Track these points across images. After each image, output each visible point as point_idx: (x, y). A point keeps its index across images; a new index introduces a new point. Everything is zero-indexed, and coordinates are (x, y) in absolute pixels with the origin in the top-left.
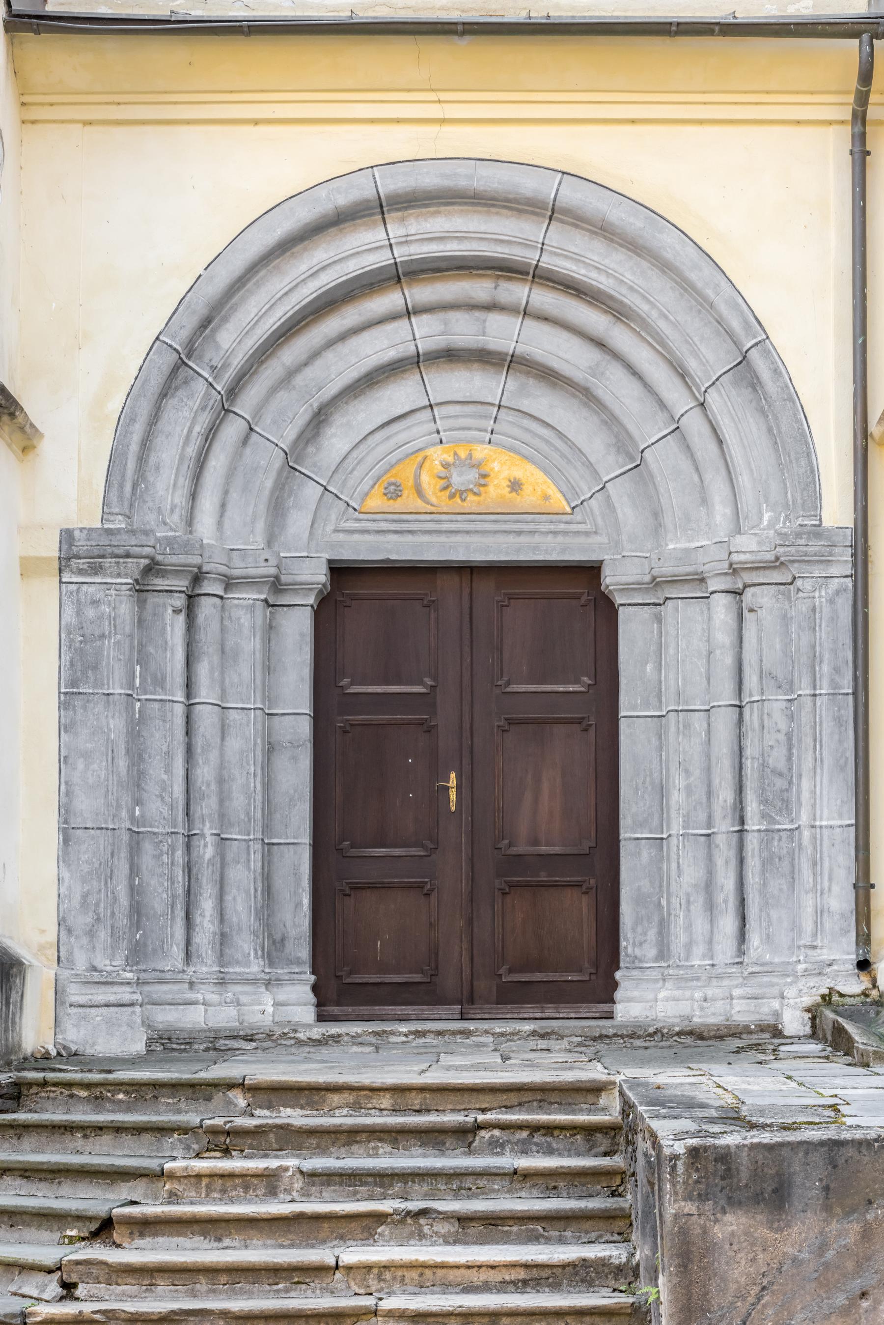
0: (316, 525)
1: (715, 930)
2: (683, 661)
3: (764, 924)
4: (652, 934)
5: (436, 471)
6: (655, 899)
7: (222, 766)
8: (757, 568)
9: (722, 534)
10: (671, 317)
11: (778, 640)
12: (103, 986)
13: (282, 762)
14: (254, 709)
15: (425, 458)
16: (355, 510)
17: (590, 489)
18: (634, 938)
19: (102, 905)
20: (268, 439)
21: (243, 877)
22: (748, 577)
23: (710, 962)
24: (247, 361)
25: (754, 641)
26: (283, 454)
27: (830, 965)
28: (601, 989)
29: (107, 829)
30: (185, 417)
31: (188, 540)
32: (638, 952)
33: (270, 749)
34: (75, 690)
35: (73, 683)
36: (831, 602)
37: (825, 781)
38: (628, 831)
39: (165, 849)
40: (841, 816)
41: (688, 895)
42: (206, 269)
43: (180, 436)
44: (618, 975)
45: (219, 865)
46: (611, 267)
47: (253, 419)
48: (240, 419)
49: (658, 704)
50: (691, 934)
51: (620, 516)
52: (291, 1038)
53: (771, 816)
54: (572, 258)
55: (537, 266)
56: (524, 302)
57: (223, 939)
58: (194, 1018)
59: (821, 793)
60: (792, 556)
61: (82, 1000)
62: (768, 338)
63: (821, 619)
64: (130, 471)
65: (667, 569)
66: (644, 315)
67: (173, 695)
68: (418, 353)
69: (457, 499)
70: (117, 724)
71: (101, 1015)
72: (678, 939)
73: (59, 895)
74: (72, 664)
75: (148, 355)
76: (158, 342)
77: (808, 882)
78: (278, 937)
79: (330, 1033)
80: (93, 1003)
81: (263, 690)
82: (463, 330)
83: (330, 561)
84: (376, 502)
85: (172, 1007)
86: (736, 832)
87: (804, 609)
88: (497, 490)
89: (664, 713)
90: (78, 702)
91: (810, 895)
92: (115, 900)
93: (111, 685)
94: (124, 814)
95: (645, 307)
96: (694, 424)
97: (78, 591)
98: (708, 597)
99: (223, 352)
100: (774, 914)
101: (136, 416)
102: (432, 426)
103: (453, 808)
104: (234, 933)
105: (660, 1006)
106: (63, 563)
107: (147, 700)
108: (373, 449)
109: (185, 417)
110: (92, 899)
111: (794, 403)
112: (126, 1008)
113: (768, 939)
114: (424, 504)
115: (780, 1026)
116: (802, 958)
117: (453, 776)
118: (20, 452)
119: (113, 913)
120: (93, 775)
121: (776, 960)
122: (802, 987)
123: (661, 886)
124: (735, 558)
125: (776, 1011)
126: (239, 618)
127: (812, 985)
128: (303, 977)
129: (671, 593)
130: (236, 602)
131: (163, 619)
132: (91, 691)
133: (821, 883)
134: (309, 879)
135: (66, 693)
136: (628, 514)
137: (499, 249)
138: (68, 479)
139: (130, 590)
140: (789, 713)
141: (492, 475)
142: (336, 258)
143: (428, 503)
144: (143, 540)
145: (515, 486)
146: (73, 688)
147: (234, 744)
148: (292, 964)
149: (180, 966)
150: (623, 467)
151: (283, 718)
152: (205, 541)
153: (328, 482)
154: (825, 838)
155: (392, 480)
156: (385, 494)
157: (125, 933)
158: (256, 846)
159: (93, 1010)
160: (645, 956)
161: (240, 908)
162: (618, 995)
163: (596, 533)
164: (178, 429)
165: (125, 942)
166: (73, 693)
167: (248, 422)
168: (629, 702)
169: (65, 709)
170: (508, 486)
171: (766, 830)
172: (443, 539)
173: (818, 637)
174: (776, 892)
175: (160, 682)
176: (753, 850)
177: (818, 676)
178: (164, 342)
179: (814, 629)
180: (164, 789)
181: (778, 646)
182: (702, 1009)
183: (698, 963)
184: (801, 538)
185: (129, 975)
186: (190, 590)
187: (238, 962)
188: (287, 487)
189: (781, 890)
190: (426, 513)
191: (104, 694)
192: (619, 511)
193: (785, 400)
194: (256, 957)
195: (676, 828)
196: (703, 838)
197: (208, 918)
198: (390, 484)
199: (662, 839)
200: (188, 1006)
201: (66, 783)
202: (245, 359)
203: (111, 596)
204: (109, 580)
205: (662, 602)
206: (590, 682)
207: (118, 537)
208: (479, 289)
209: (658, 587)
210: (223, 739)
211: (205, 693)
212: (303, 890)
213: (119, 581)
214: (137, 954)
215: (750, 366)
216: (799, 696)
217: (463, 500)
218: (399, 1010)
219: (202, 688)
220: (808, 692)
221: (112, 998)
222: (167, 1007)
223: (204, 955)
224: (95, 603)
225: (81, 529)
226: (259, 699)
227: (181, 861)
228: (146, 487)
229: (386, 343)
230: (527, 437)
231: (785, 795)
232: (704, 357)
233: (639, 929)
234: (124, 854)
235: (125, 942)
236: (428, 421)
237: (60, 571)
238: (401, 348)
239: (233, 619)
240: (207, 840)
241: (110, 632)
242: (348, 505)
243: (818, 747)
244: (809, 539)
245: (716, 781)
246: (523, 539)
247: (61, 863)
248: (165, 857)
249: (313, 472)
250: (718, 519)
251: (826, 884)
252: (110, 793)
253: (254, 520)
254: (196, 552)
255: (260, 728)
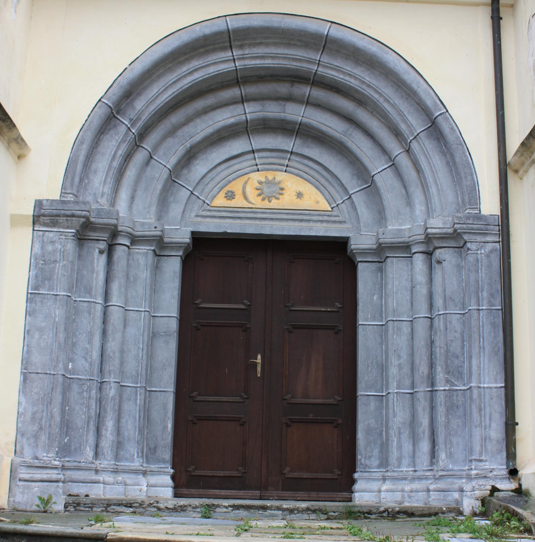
0: (185, 212)
1: (417, 449)
2: (396, 292)
3: (448, 446)
4: (376, 452)
5: (255, 186)
6: (378, 431)
7: (123, 343)
8: (442, 238)
9: (420, 220)
10: (391, 101)
11: (455, 279)
12: (40, 469)
13: (160, 343)
14: (144, 311)
15: (249, 178)
16: (208, 205)
17: (342, 198)
18: (366, 454)
19: (44, 420)
20: (160, 163)
21: (132, 409)
22: (437, 244)
23: (413, 469)
24: (150, 118)
25: (440, 279)
26: (168, 171)
27: (491, 472)
28: (347, 484)
29: (50, 374)
30: (113, 145)
31: (110, 210)
32: (367, 462)
33: (153, 336)
34: (36, 292)
35: (36, 288)
36: (488, 256)
37: (486, 361)
38: (364, 391)
39: (85, 388)
40: (496, 382)
41: (399, 429)
42: (130, 65)
43: (110, 155)
44: (356, 475)
45: (118, 401)
46: (357, 74)
47: (153, 151)
48: (145, 150)
49: (380, 318)
50: (401, 452)
51: (359, 212)
52: (155, 507)
53: (452, 382)
54: (335, 69)
55: (315, 73)
56: (307, 94)
57: (119, 445)
58: (97, 492)
59: (484, 367)
60: (464, 230)
61: (27, 476)
62: (447, 111)
63: (482, 265)
64: (79, 170)
65: (387, 239)
66: (376, 101)
67: (96, 299)
68: (247, 120)
69: (266, 201)
70: (59, 313)
71: (38, 487)
72: (394, 454)
73: (18, 413)
74: (36, 276)
75: (94, 108)
76: (100, 103)
77: (477, 420)
78: (152, 446)
79: (179, 504)
80: (34, 479)
81: (150, 303)
82: (273, 111)
83: (193, 233)
84: (220, 201)
85: (84, 484)
86: (429, 391)
87: (472, 260)
88: (287, 201)
89: (384, 323)
90: (38, 299)
91: (478, 429)
92: (52, 416)
93: (59, 290)
94: (61, 365)
95: (376, 96)
96: (404, 161)
97: (43, 235)
98: (411, 257)
99: (137, 111)
100: (454, 440)
101: (84, 140)
102: (253, 162)
103: (259, 375)
104: (126, 442)
105: (383, 495)
106: (35, 219)
107: (80, 301)
108: (220, 172)
109: (113, 145)
110: (38, 416)
111: (463, 146)
112: (53, 484)
113: (450, 456)
114: (247, 203)
115: (461, 509)
116: (473, 467)
117: (259, 357)
118: (16, 158)
119: (50, 425)
120: (43, 342)
121: (456, 468)
122: (475, 485)
123: (382, 424)
124: (429, 231)
125: (457, 500)
126: (138, 260)
127: (481, 484)
128: (166, 470)
129: (389, 254)
130: (137, 250)
131: (93, 256)
132: (46, 293)
133: (485, 421)
134: (172, 412)
135: (31, 293)
136: (364, 212)
137: (295, 64)
138: (44, 176)
139: (73, 236)
140: (462, 321)
141: (286, 188)
142: (203, 65)
143: (250, 203)
144: (83, 207)
145: (300, 195)
146: (36, 290)
147: (131, 331)
148: (160, 462)
149: (91, 459)
150: (361, 186)
151: (161, 319)
152: (121, 215)
153: (194, 189)
154: (487, 395)
155: (230, 189)
156: (226, 197)
157: (56, 437)
158: (141, 391)
159: (33, 484)
160: (372, 465)
161: (129, 427)
162: (357, 487)
163: (345, 222)
164: (109, 151)
165: (57, 442)
166: (35, 293)
167: (150, 153)
168: (365, 319)
169: (30, 302)
170: (296, 195)
171: (449, 390)
172: (257, 222)
173: (480, 276)
174: (455, 427)
175: (89, 291)
176: (441, 402)
177: (481, 299)
178: (103, 102)
179: (478, 272)
180: (87, 354)
181: (455, 282)
182: (410, 497)
183: (406, 469)
184: (469, 220)
185: (57, 463)
186: (110, 241)
187: (127, 460)
188: (170, 191)
189: (458, 426)
190: (249, 208)
191: (54, 295)
192: (358, 210)
193: (458, 144)
194: (138, 457)
195: (393, 389)
196: (408, 395)
197: (109, 432)
198: (229, 192)
199: (383, 396)
200: (93, 484)
201: (28, 346)
202: (149, 116)
203: (62, 239)
204: (62, 230)
205: (383, 261)
206: (340, 306)
207: (68, 205)
208: (283, 89)
209: (382, 252)
210: (125, 327)
211: (116, 300)
212: (169, 419)
213: (67, 230)
214: (65, 450)
215: (437, 128)
216: (470, 310)
217: (270, 202)
218: (223, 492)
219: (114, 297)
220: (475, 307)
221: (45, 477)
222: (81, 484)
223: (106, 454)
224: (53, 242)
225: (47, 200)
226: (147, 306)
227: (95, 396)
228: (88, 182)
229: (229, 115)
230: (307, 170)
231: (460, 369)
232: (410, 123)
233: (369, 449)
234: (59, 390)
235: (57, 442)
236: (252, 159)
237: (34, 223)
238: (238, 118)
239: (135, 260)
240: (112, 385)
241: (60, 259)
242: (204, 202)
243: (481, 340)
244: (474, 220)
245: (417, 361)
246: (303, 224)
247: (21, 393)
248: (85, 394)
249: (185, 183)
250: (418, 212)
251: (488, 422)
252: (53, 353)
253: (150, 206)
254: (114, 218)
255: (147, 322)
